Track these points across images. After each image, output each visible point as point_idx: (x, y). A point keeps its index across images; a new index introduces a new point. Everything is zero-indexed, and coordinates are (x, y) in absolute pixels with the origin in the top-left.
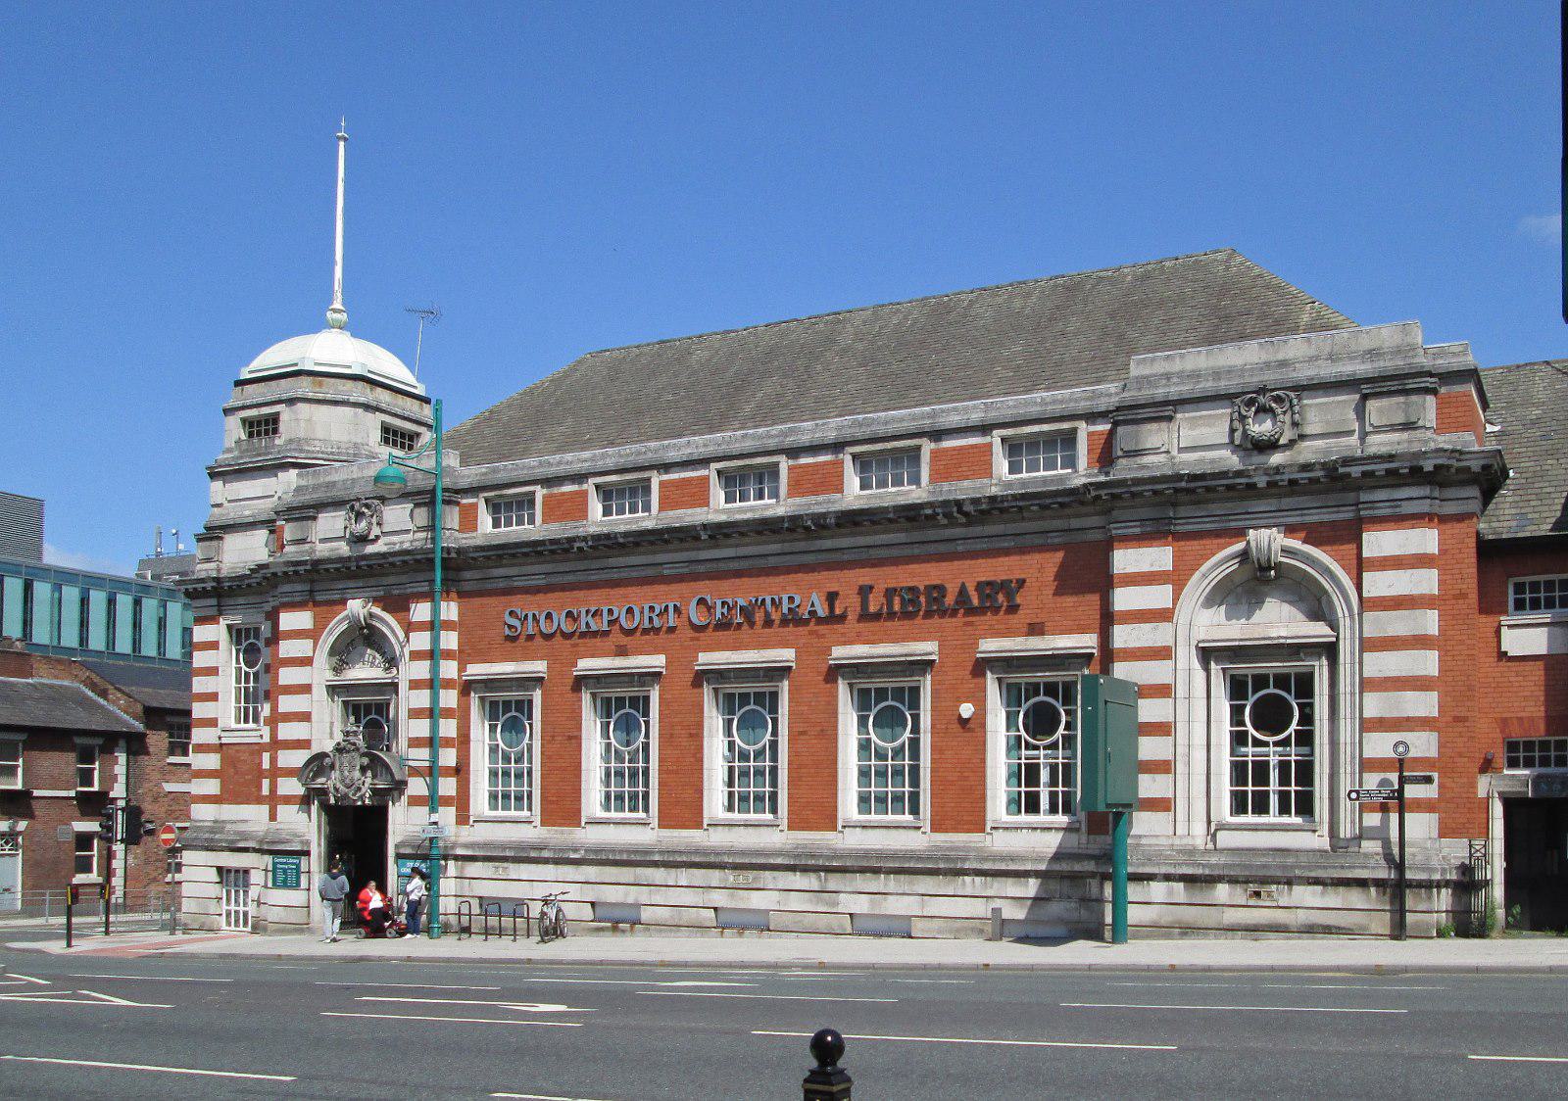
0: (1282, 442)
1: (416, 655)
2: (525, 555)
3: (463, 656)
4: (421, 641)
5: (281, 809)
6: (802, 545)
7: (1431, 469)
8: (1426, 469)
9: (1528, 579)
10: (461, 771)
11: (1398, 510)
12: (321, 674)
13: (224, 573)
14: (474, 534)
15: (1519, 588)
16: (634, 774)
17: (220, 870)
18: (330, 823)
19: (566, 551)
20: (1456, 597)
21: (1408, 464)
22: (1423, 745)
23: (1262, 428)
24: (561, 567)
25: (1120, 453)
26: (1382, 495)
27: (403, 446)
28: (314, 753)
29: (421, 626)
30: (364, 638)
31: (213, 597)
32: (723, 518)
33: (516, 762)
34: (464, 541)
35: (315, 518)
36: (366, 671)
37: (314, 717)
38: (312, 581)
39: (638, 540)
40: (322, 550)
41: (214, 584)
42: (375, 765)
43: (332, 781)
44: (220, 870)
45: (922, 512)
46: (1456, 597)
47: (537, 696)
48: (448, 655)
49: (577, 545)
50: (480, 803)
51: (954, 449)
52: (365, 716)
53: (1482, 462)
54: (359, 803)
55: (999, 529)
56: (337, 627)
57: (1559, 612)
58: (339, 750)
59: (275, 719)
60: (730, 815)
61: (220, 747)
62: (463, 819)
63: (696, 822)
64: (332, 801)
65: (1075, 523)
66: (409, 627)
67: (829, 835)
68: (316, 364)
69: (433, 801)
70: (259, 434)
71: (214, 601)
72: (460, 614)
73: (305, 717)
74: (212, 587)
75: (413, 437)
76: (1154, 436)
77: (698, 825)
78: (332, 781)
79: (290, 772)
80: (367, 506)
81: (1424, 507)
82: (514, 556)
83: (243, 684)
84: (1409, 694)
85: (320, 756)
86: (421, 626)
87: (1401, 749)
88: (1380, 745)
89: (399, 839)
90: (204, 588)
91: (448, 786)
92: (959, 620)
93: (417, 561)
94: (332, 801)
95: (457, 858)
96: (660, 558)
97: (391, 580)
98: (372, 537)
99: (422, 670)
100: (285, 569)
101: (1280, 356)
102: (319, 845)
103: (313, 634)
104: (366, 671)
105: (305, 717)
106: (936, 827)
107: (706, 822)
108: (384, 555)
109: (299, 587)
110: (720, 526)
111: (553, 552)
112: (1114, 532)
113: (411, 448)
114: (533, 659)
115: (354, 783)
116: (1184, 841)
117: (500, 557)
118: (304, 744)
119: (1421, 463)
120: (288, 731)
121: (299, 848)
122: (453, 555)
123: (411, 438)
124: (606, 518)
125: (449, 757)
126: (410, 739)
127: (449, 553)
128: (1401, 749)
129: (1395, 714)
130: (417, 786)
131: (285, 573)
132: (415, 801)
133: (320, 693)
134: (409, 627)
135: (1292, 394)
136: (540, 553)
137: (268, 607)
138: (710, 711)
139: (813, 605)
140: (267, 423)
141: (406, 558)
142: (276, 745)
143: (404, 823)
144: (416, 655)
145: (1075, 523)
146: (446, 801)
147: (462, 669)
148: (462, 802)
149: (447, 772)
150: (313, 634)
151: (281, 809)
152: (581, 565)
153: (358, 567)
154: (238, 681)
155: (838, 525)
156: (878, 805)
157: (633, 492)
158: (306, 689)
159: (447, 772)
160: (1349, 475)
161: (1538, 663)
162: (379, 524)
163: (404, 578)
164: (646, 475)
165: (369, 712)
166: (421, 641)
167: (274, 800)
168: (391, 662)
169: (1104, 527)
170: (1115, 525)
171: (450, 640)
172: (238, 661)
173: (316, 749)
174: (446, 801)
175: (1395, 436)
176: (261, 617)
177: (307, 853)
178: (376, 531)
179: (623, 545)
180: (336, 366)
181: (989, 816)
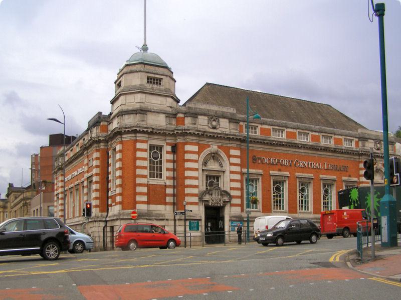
16: (277, 202)
23: (214, 123)
27: (157, 83)
30: (214, 156)
36: (213, 166)
37: (229, 181)
40: (200, 128)
56: (207, 151)
61: (148, 185)
66: (229, 156)
70: (151, 83)
73: (232, 180)
75: (161, 80)
78: (207, 197)
82: (258, 142)
92: (339, 172)
93: (237, 138)
97: (223, 141)
103: (199, 153)
104: (213, 166)
105: (232, 180)
111: (267, 143)
113: (160, 84)
114: (259, 169)
123: (160, 81)
140: (157, 80)
150: (199, 153)
155: (324, 150)
156: (28, 228)
158: (232, 172)
161: (187, 158)
163: (227, 142)
164: (284, 128)
177: (200, 220)
178: (218, 127)
179: (283, 145)
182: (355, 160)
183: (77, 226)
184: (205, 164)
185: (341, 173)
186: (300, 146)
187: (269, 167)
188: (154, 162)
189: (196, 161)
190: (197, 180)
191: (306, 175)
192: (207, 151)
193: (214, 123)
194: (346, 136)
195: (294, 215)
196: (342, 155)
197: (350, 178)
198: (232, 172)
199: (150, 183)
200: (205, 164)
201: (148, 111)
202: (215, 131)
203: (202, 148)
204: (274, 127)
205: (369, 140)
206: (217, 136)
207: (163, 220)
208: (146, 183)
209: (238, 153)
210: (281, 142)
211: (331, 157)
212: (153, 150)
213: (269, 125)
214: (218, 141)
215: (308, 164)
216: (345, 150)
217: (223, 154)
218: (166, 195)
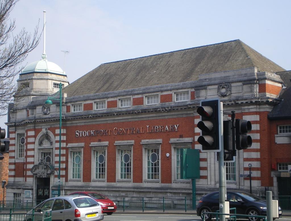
0: (227, 95)
1: (57, 142)
2: (80, 118)
3: (67, 142)
4: (58, 138)
5: (28, 179)
6: (135, 117)
7: (254, 102)
8: (253, 102)
9: (282, 126)
10: (66, 169)
11: (249, 111)
12: (36, 146)
13: (17, 120)
14: (92, 111)
15: (280, 128)
17: (14, 194)
18: (37, 182)
19: (88, 117)
20: (263, 130)
21: (249, 101)
22: (256, 164)
23: (223, 91)
24: (87, 121)
25: (196, 97)
26: (246, 107)
28: (35, 165)
29: (57, 135)
31: (14, 127)
32: (120, 110)
33: (284, 167)
34: (67, 115)
35: (36, 109)
36: (46, 145)
38: (35, 124)
39: (102, 115)
40: (37, 116)
41: (14, 124)
42: (47, 167)
43: (37, 171)
44: (14, 194)
45: (158, 110)
46: (263, 130)
47: (82, 150)
48: (63, 141)
49: (90, 116)
50: (70, 176)
51: (165, 95)
52: (46, 156)
53: (266, 100)
54: (44, 177)
55: (173, 113)
57: (289, 134)
58: (40, 164)
59: (27, 157)
60: (97, 179)
62: (67, 180)
63: (114, 181)
64: (38, 177)
65: (189, 112)
66: (55, 135)
67: (141, 184)
68: (50, 70)
69: (59, 176)
71: (14, 128)
72: (66, 132)
74: (14, 125)
76: (203, 93)
77: (115, 182)
79: (29, 170)
80: (226, 85)
81: (254, 110)
83: (21, 148)
84: (253, 153)
85: (36, 165)
86: (57, 135)
87: (250, 165)
88: (246, 164)
89: (52, 185)
90: (12, 125)
91: (63, 173)
93: (57, 120)
94: (38, 177)
95: (65, 190)
96: (107, 119)
97: (52, 124)
98: (47, 113)
99: (57, 145)
100: (29, 121)
101: (210, 77)
102: (35, 187)
103: (35, 137)
104: (46, 145)
106: (162, 182)
107: (116, 180)
108: (49, 118)
109: (32, 125)
110: (118, 112)
111: (85, 117)
112: (195, 115)
115: (41, 172)
116: (210, 186)
117: (74, 118)
118: (33, 163)
119: (252, 101)
120: (30, 160)
121: (31, 188)
122: (64, 118)
124: (67, 113)
125: (63, 166)
126: (55, 161)
127: (63, 118)
128: (250, 165)
129: (250, 157)
130: (56, 173)
131: (29, 122)
132: (56, 176)
133: (36, 150)
134: (55, 135)
135: (229, 84)
136: (82, 118)
137: (26, 129)
138: (117, 155)
139: (166, 128)
141: (54, 119)
142: (27, 163)
143: (54, 181)
144: (57, 142)
145: (189, 112)
146: (63, 176)
147: (67, 145)
148: (66, 176)
149: (63, 169)
151: (28, 179)
152: (91, 120)
153: (44, 121)
154: (20, 147)
155: (142, 112)
157: (127, 100)
159: (63, 169)
160: (238, 103)
162: (49, 110)
163: (54, 123)
164: (104, 100)
165: (47, 155)
166: (58, 138)
167: (26, 176)
168: (51, 143)
169: (193, 113)
170: (195, 113)
171: (64, 138)
172: (20, 143)
173: (35, 164)
174: (63, 176)
175: (237, 94)
176: (24, 132)
179: (99, 116)
180: (55, 71)
181: (143, 179)
182: (189, 115)
183: (128, 193)
184: (41, 143)
185: (168, 135)
186: (115, 114)
187: (90, 139)
188: (22, 145)
189: (34, 143)
190: (33, 158)
191: (126, 141)
192: (40, 135)
193: (223, 91)
194: (177, 89)
195: (112, 183)
196: (169, 114)
197: (181, 139)
198: (33, 150)
199: (16, 162)
200: (41, 143)
201: (18, 110)
202: (47, 116)
203: (37, 131)
204: (119, 98)
205: (210, 87)
206: (44, 121)
207: (20, 189)
208: (14, 162)
209: (64, 131)
210: (96, 114)
211: (155, 118)
212: (22, 137)
213: (91, 100)
214: (48, 124)
215: (80, 134)
216: (168, 107)
217: (51, 134)
218: (27, 170)
